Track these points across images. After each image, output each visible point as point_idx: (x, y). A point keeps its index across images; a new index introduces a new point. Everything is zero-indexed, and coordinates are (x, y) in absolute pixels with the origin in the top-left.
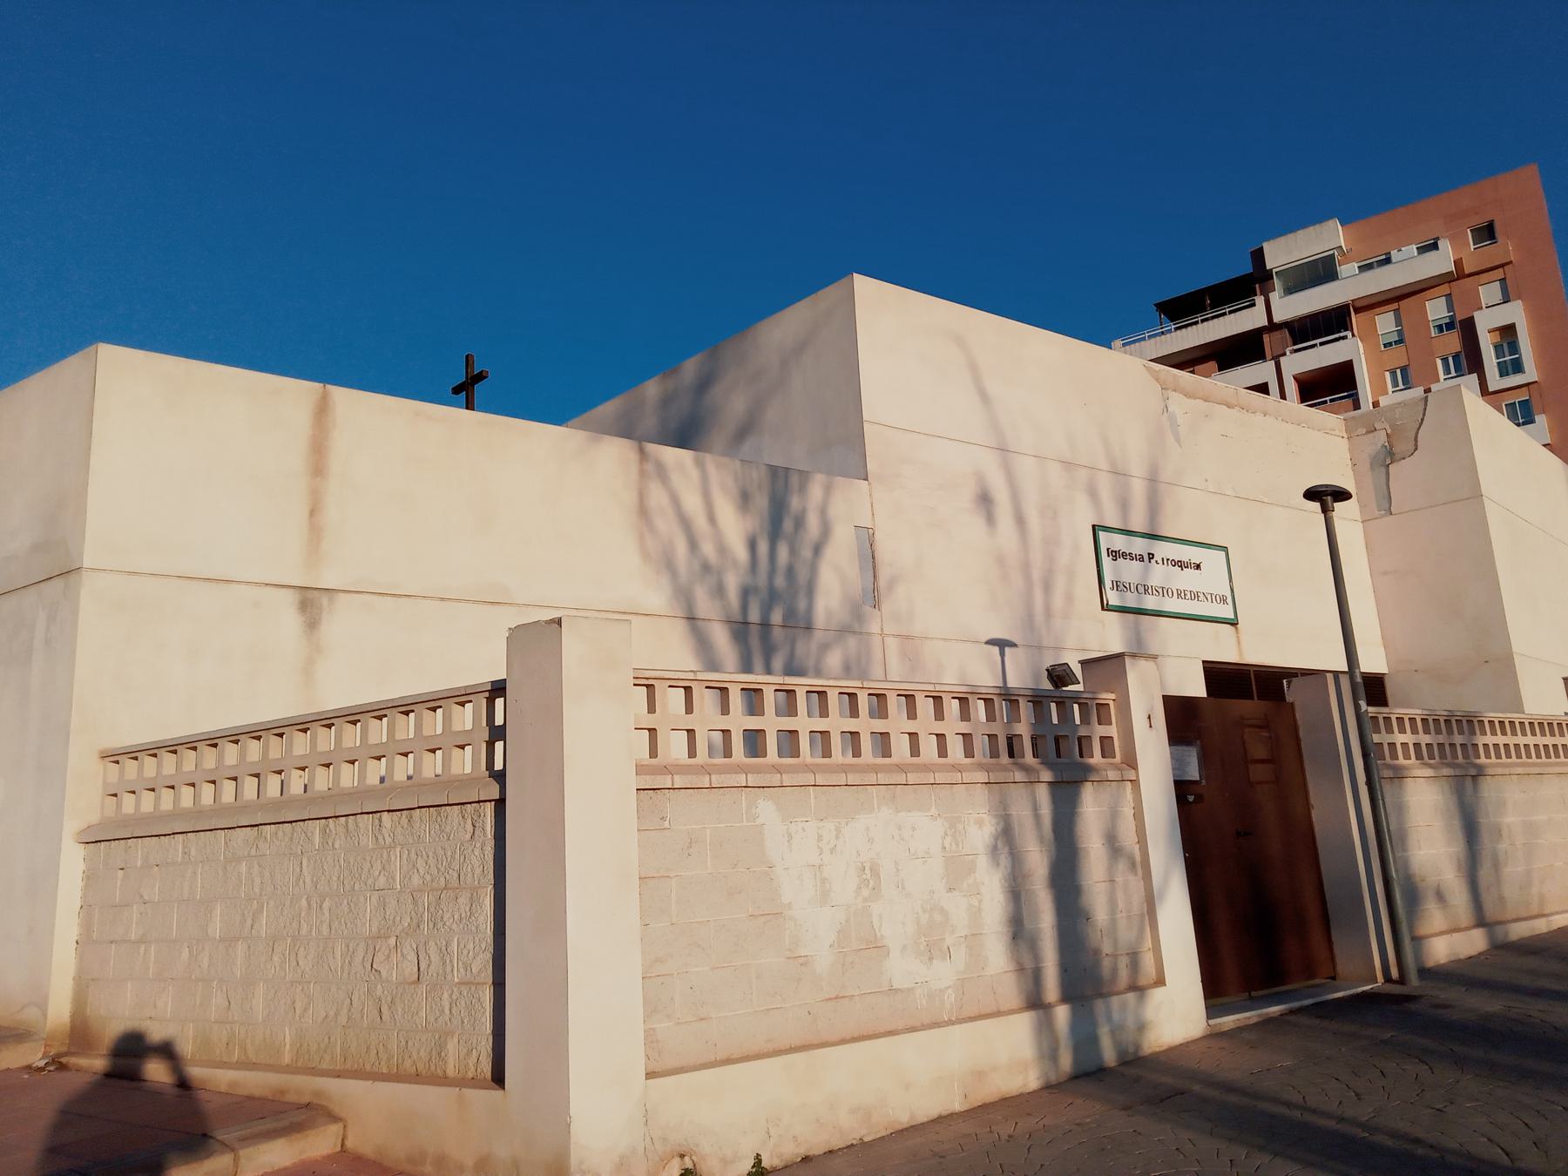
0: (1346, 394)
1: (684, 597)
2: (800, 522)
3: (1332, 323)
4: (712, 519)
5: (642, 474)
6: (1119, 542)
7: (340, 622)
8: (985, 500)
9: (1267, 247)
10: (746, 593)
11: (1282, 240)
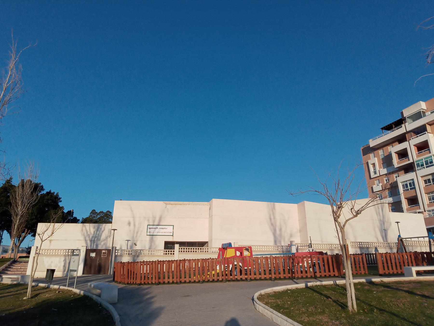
0: (427, 149)
1: (85, 238)
2: (101, 229)
3: (421, 130)
4: (90, 230)
5: (83, 227)
6: (151, 227)
7: (53, 242)
8: (129, 224)
9: (403, 111)
10: (92, 237)
11: (405, 109)
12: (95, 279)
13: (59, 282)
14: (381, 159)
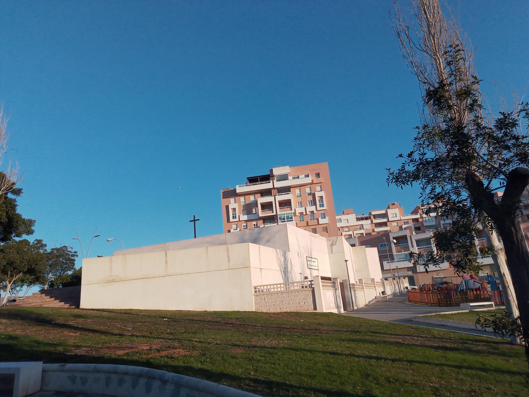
3: (286, 190)
12: (478, 309)
13: (371, 312)
14: (242, 206)
